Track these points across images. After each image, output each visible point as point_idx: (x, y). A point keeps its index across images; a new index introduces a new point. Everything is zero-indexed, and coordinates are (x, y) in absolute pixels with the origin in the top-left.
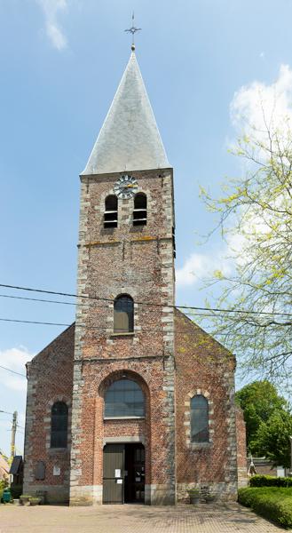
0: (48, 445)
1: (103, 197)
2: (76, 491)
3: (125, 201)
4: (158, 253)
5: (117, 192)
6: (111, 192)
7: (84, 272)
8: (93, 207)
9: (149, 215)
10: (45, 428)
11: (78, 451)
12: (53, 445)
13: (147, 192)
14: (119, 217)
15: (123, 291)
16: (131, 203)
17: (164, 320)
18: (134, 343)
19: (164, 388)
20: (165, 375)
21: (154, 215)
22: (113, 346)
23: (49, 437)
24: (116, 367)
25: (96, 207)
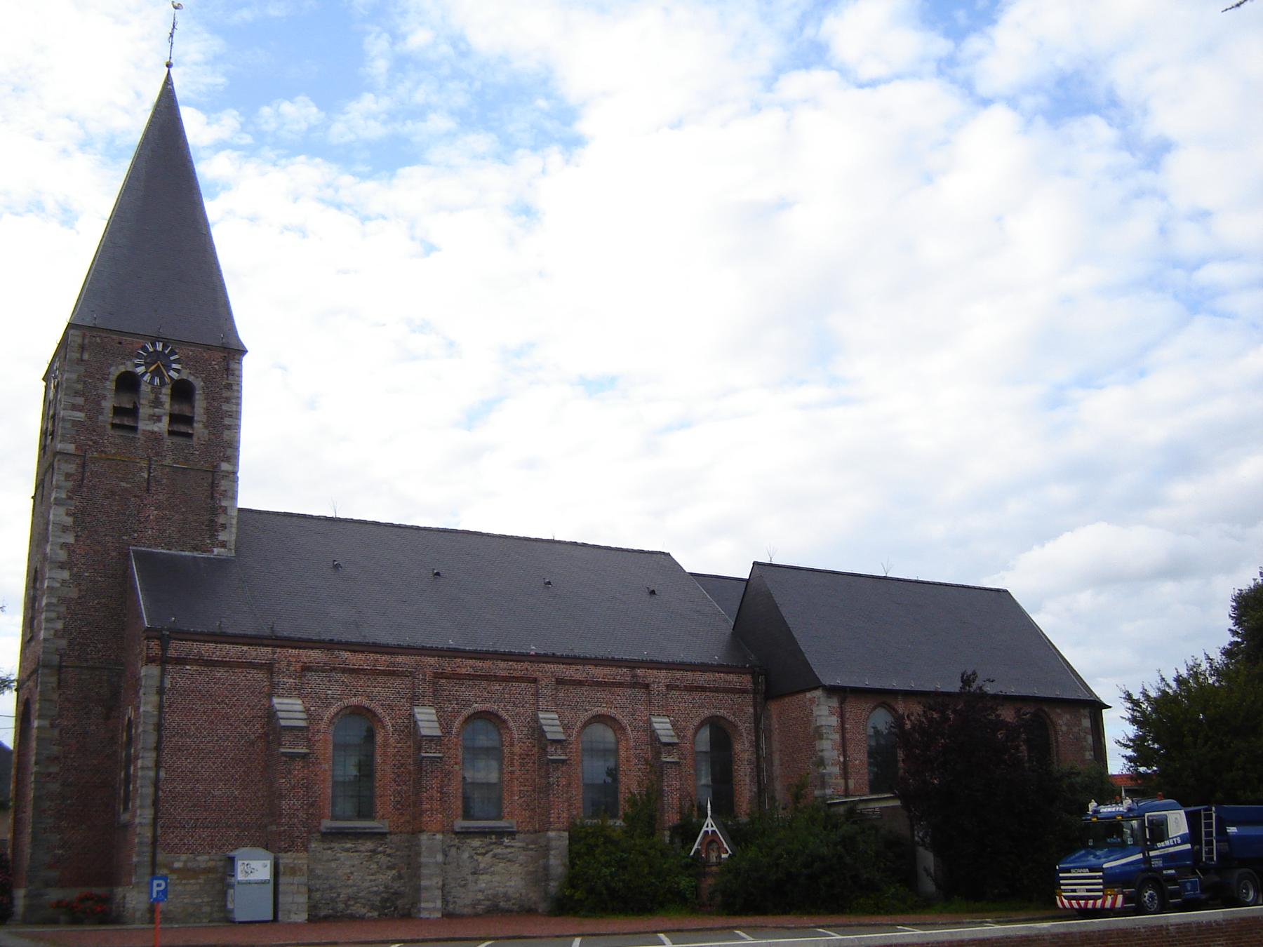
5: (141, 370)
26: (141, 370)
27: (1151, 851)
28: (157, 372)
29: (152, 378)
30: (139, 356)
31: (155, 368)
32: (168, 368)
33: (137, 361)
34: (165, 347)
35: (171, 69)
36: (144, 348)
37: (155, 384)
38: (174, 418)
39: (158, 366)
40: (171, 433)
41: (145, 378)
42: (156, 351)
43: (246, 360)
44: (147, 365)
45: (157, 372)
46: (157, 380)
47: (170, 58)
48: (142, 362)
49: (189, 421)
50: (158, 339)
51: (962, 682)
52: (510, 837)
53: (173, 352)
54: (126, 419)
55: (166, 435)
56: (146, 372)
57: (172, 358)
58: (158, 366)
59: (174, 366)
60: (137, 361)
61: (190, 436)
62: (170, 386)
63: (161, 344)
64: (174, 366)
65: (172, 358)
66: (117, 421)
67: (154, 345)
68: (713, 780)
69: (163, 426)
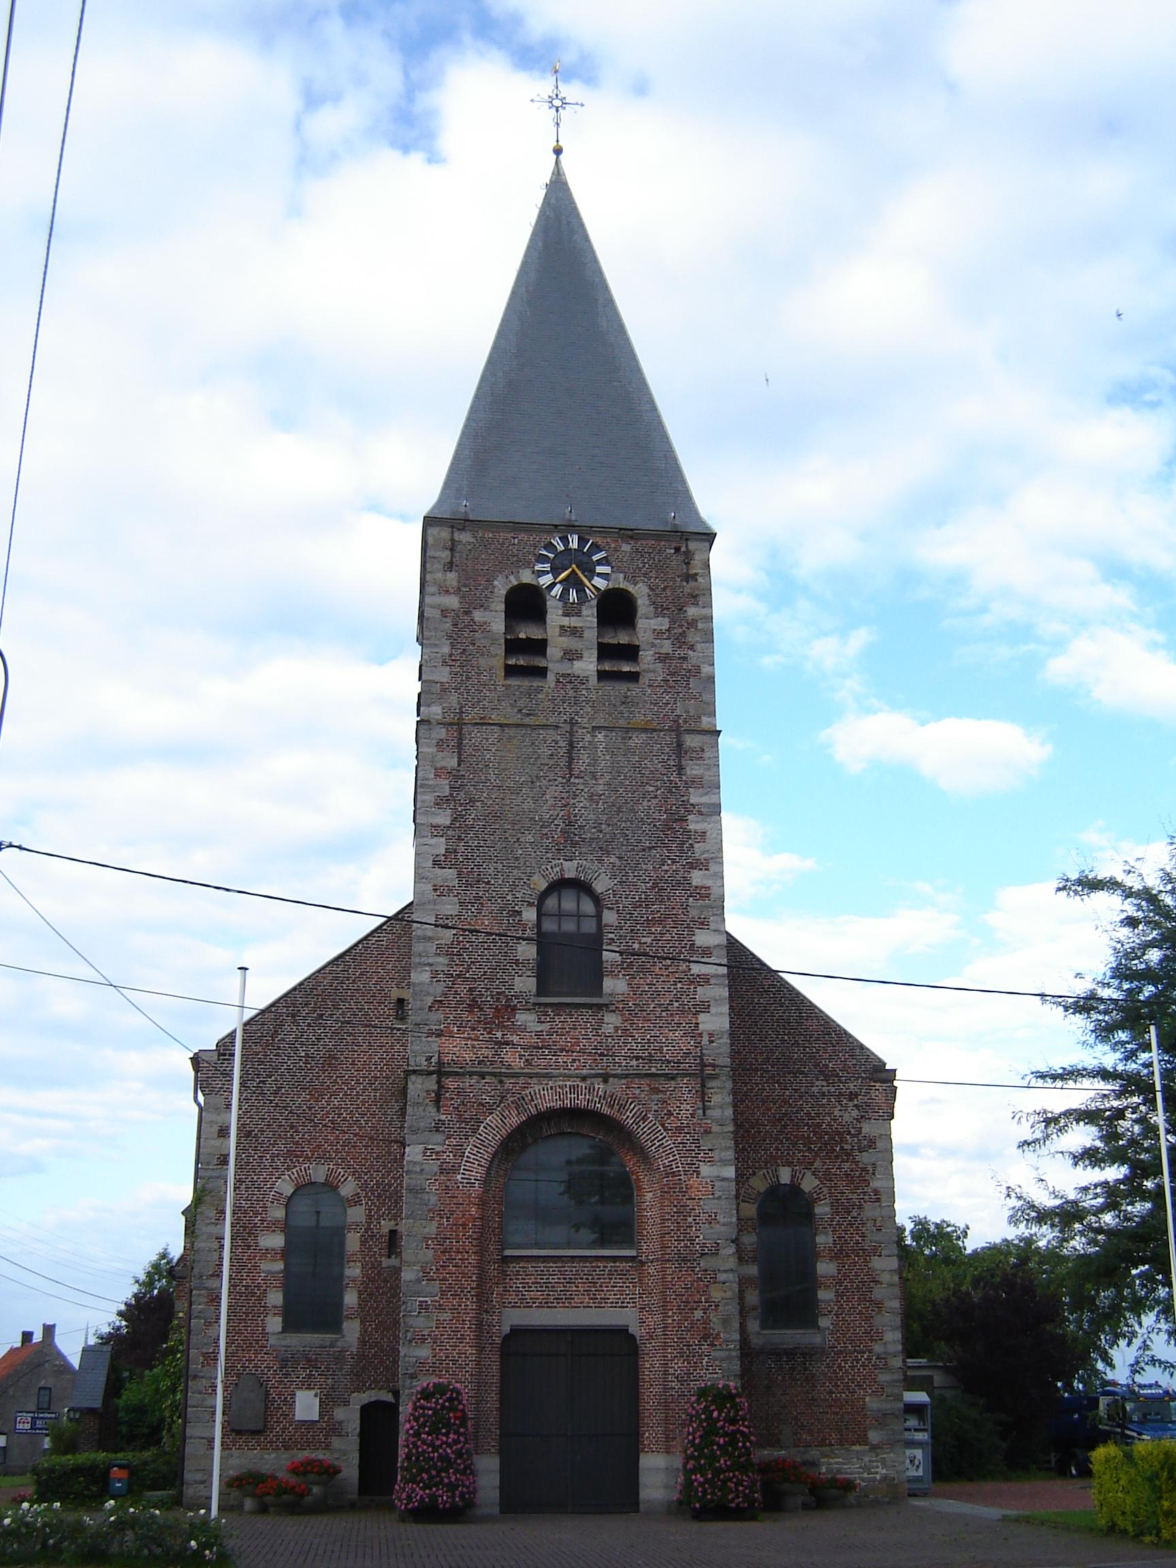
0: (274, 1323)
1: (501, 587)
2: (493, 606)
3: (570, 610)
4: (680, 769)
5: (546, 580)
6: (526, 577)
7: (440, 802)
8: (467, 613)
9: (646, 656)
10: (265, 1266)
11: (424, 1352)
12: (292, 1323)
13: (640, 592)
14: (553, 651)
15: (570, 870)
16: (589, 617)
17: (702, 993)
18: (608, 1029)
19: (705, 1170)
20: (708, 1132)
21: (663, 658)
22: (539, 1034)
23: (275, 1298)
24: (547, 1097)
25: (478, 616)
26: (546, 580)
27: (1155, 1088)
28: (573, 582)
29: (565, 592)
30: (542, 559)
31: (569, 576)
32: (591, 573)
33: (538, 567)
34: (583, 542)
35: (562, 157)
36: (550, 546)
37: (571, 601)
38: (605, 652)
39: (573, 570)
40: (602, 675)
41: (553, 593)
42: (568, 550)
43: (717, 556)
44: (555, 571)
45: (573, 582)
46: (573, 596)
47: (558, 141)
48: (547, 567)
49: (631, 652)
50: (571, 527)
51: (217, 1046)
52: (1149, 1179)
53: (596, 548)
54: (606, 664)
55: (593, 680)
56: (553, 585)
57: (595, 558)
58: (573, 570)
59: (599, 569)
60: (538, 567)
61: (633, 677)
62: (594, 602)
63: (576, 537)
64: (599, 569)
65: (595, 558)
66: (607, 667)
67: (565, 540)
68: (341, 1324)
69: (588, 665)
